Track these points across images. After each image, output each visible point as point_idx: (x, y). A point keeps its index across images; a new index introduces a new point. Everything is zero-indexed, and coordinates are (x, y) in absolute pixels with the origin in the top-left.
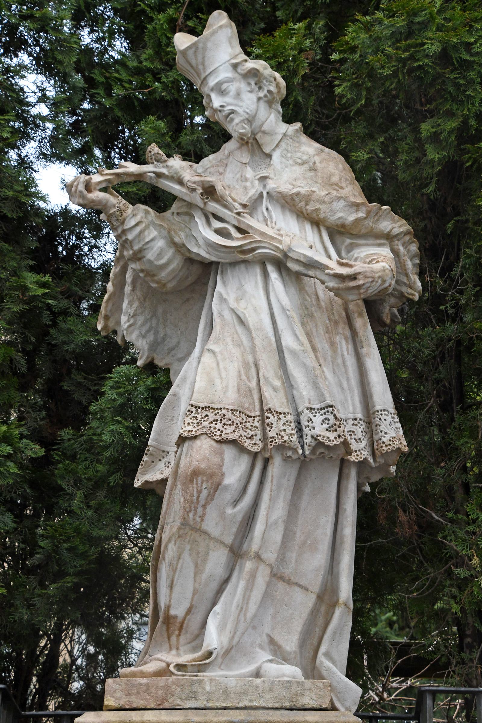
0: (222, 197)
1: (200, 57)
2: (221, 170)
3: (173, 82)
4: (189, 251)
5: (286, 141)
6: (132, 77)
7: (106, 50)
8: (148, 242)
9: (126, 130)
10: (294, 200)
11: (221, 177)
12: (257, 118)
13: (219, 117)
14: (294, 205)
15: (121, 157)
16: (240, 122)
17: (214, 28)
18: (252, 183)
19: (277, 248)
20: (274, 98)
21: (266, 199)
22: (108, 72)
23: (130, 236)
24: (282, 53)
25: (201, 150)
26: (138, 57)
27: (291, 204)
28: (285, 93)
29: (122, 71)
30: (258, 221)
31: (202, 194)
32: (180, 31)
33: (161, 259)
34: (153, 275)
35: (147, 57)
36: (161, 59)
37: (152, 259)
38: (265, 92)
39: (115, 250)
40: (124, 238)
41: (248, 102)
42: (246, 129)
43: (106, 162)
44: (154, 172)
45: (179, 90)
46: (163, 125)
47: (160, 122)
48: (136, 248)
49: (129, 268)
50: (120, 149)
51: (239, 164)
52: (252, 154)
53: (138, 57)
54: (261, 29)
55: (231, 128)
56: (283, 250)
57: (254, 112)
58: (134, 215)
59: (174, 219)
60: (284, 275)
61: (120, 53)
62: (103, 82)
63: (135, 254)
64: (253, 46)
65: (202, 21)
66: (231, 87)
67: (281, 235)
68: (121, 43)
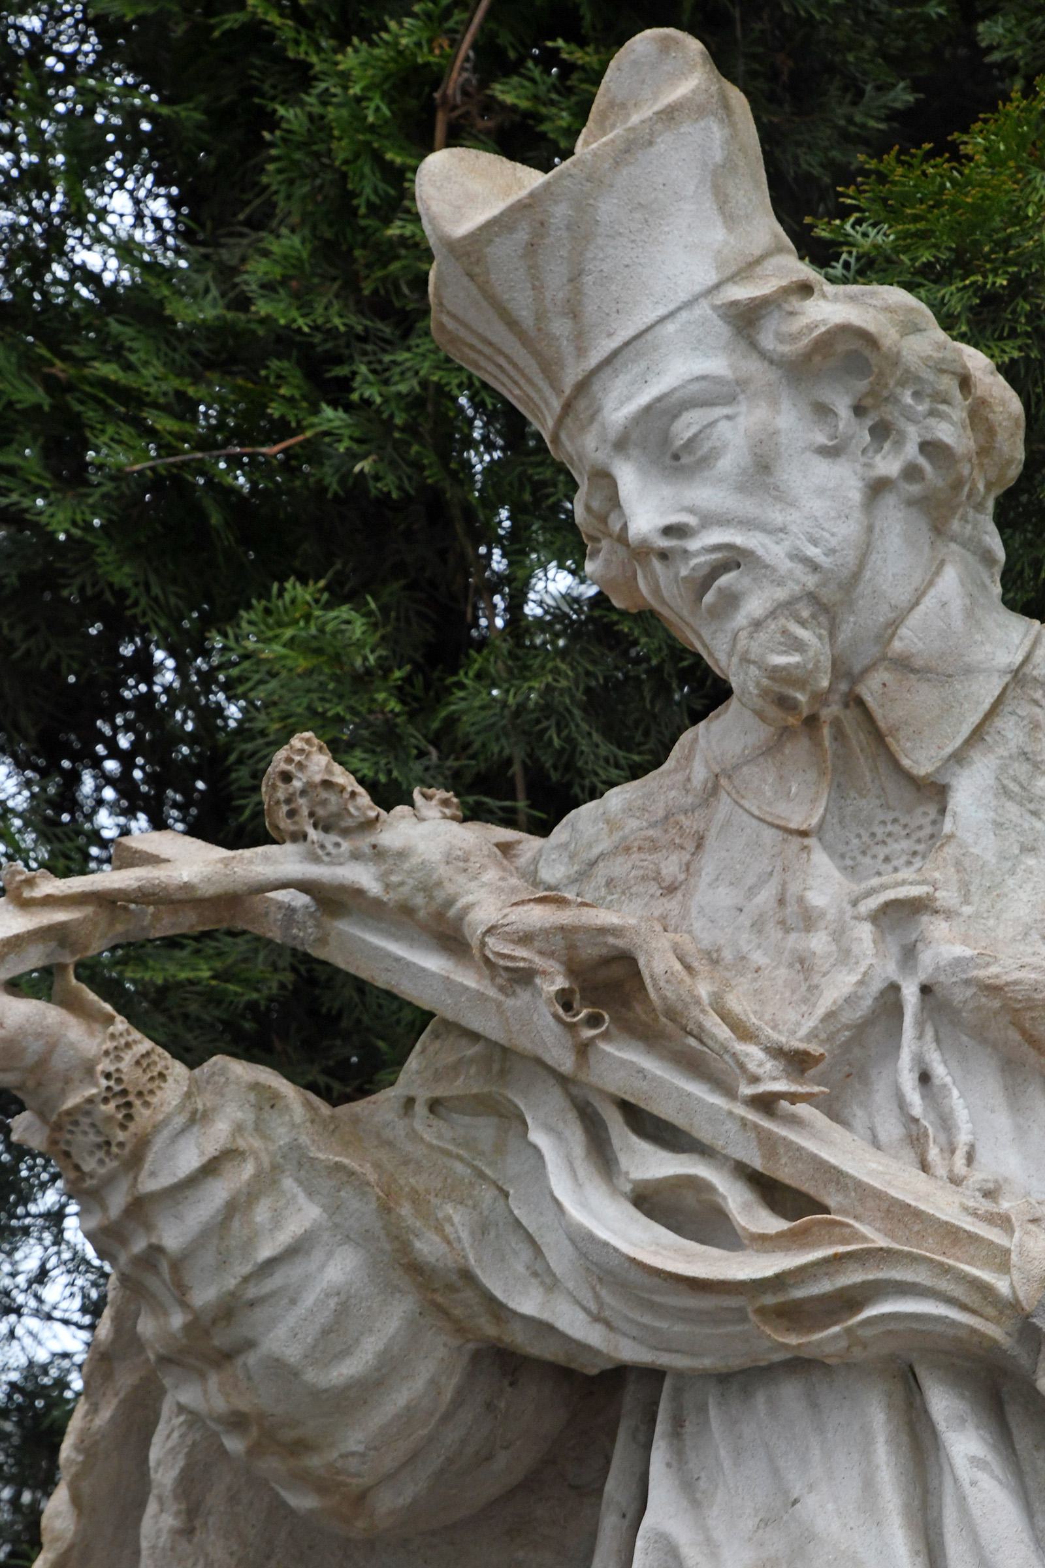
0: (672, 1014)
1: (555, 276)
2: (671, 866)
3: (415, 403)
4: (497, 1309)
5: (1025, 709)
6: (197, 380)
7: (56, 238)
8: (272, 1263)
9: (159, 655)
11: (671, 905)
12: (863, 588)
13: (659, 587)
15: (132, 801)
16: (772, 614)
17: (635, 119)
18: (839, 935)
19: (984, 1289)
20: (957, 485)
21: (920, 1025)
22: (67, 357)
23: (173, 1235)
24: (1005, 244)
25: (568, 760)
26: (227, 273)
28: (1020, 455)
29: (140, 348)
30: (876, 1143)
31: (565, 1000)
32: (453, 140)
33: (346, 1353)
34: (300, 1447)
35: (277, 272)
36: (351, 284)
37: (293, 1353)
38: (911, 450)
39: (93, 1308)
40: (139, 1245)
41: (818, 506)
42: (804, 650)
43: (48, 830)
44: (304, 886)
45: (449, 438)
46: (358, 628)
47: (344, 611)
48: (204, 1295)
49: (167, 1408)
50: (127, 759)
51: (769, 834)
52: (841, 779)
53: (227, 273)
54: (893, 116)
55: (719, 649)
56: (1014, 1305)
57: (851, 557)
58: (197, 1119)
59: (414, 1136)
60: (1023, 1440)
61: (126, 250)
62: (38, 407)
63: (198, 1327)
64: (844, 212)
65: (574, 80)
66: (723, 426)
67: (1004, 1222)
68: (137, 202)
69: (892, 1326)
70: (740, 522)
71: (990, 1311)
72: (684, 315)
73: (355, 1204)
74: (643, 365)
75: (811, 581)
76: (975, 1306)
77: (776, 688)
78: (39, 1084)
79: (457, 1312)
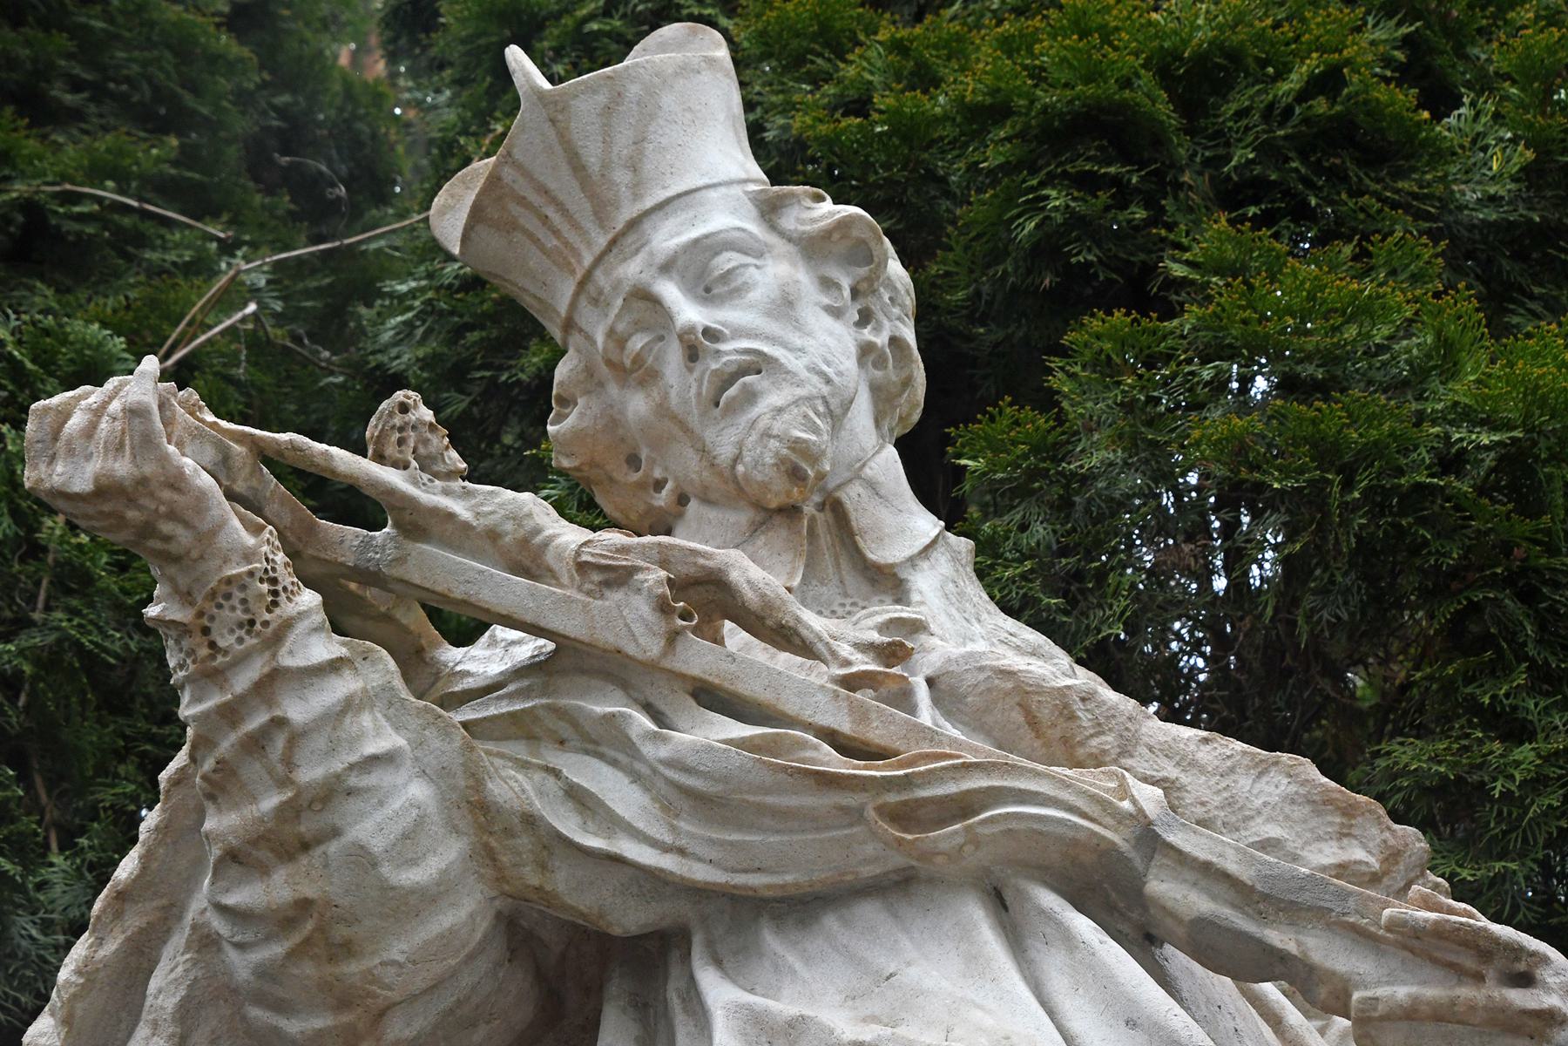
10: (1072, 717)
14: (1065, 740)
23: (298, 709)
27: (1055, 734)
33: (413, 862)
37: (377, 845)
48: (310, 773)
66: (752, 270)
69: (1014, 825)
70: (767, 338)
71: (1109, 820)
72: (723, 190)
73: (436, 743)
74: (691, 214)
75: (825, 390)
76: (1095, 815)
77: (793, 457)
78: (202, 557)
79: (505, 859)
